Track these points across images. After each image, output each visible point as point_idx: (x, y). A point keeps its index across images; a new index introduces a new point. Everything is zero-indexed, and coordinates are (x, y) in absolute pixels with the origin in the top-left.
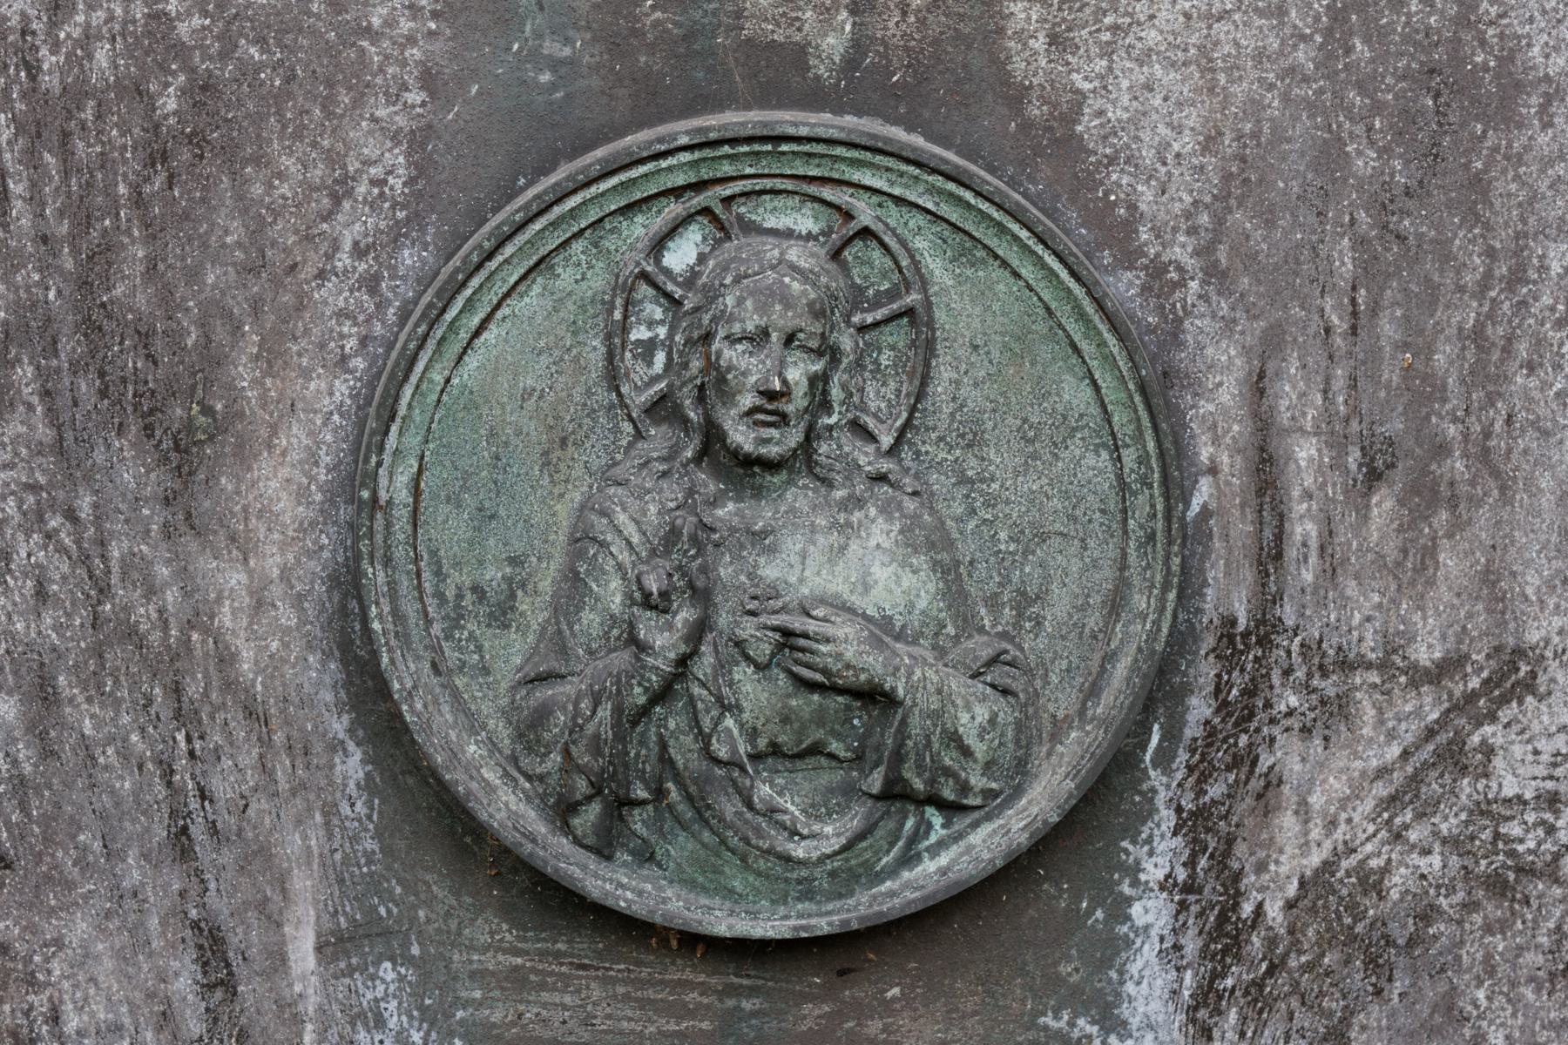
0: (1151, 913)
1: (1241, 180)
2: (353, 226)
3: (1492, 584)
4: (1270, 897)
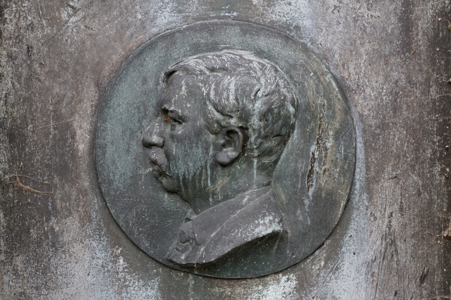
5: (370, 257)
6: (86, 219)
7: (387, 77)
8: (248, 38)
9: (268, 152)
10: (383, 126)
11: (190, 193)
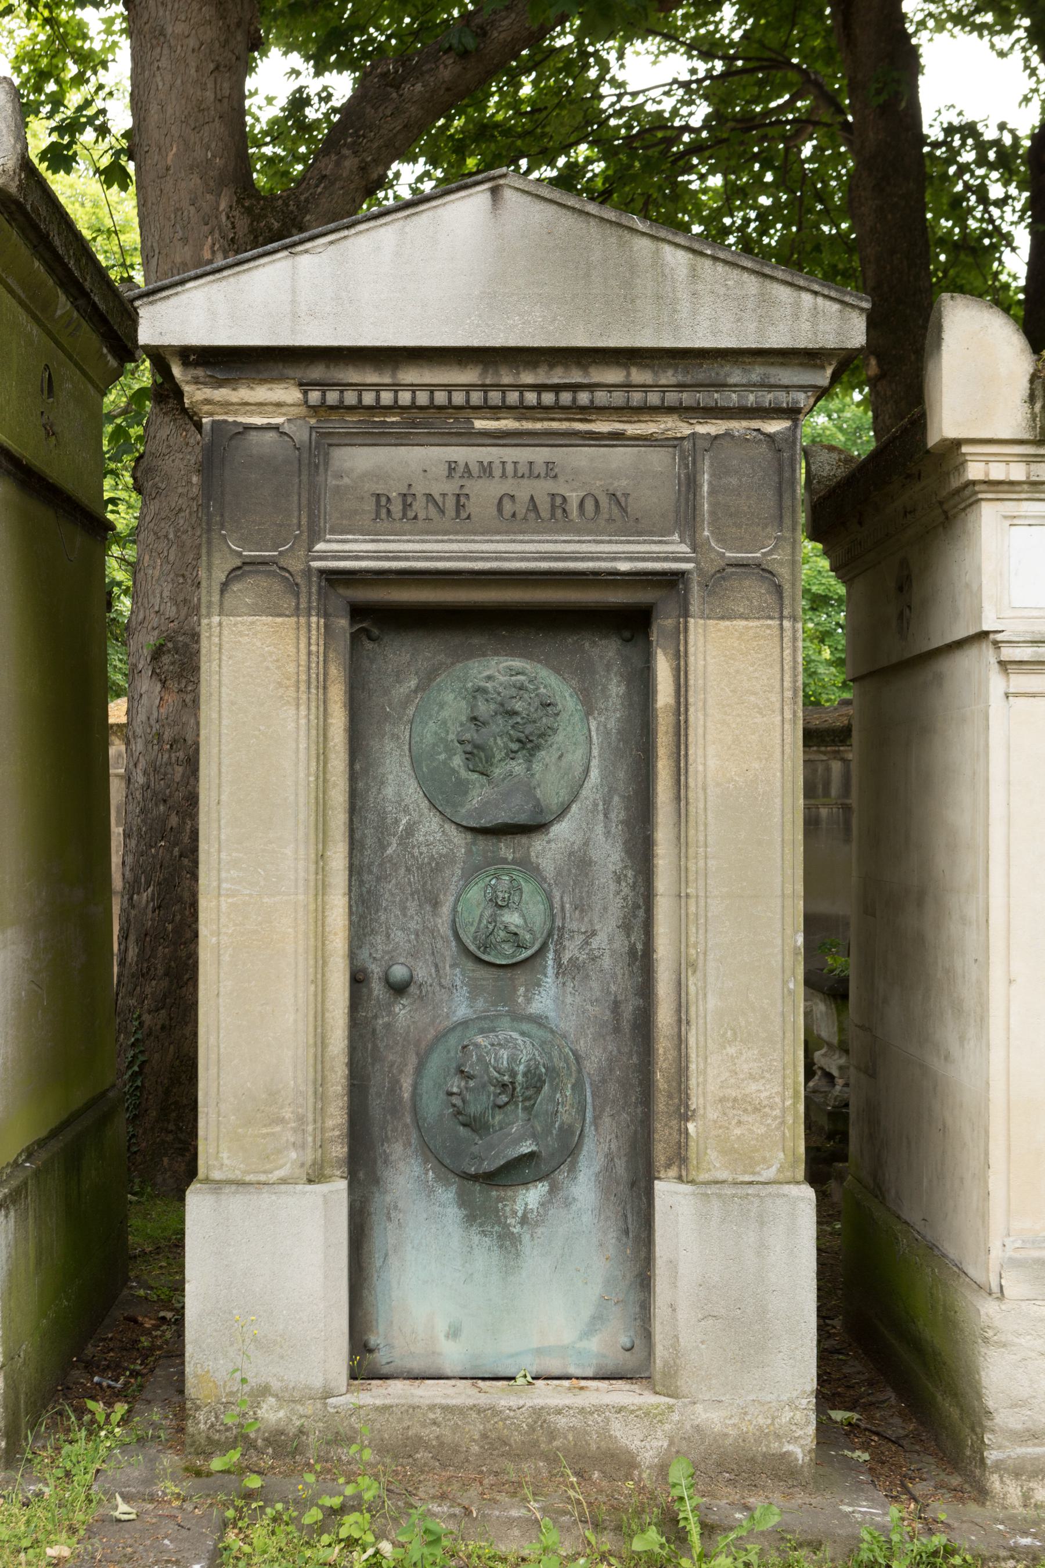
0: (550, 962)
1: (559, 873)
2: (455, 879)
3: (591, 921)
4: (565, 961)
5: (597, 1169)
6: (407, 1144)
7: (605, 1049)
8: (515, 1024)
9: (528, 1099)
10: (604, 1081)
11: (476, 1125)
